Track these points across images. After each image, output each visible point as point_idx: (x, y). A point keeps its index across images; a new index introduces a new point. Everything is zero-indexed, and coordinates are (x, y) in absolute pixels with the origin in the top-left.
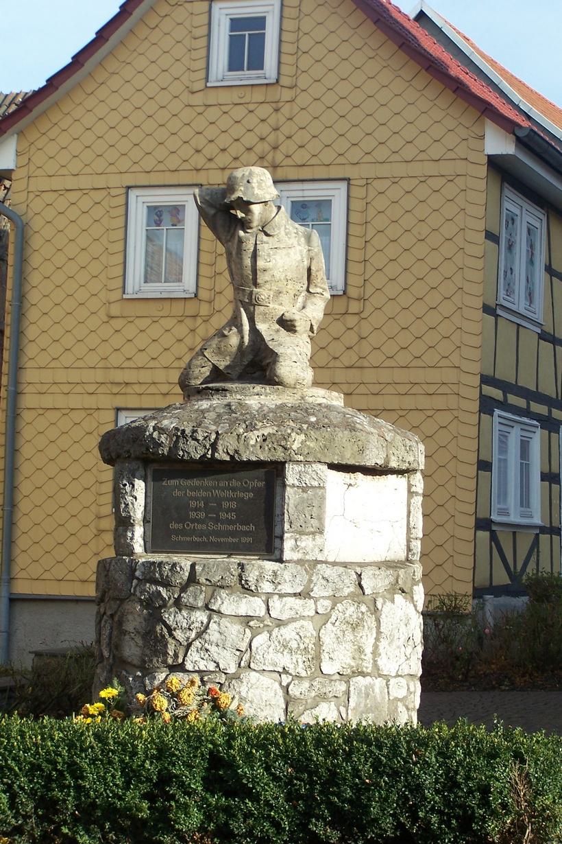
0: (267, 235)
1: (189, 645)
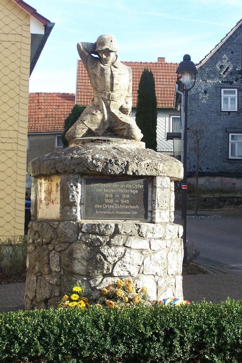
0: (115, 67)
1: (115, 264)
